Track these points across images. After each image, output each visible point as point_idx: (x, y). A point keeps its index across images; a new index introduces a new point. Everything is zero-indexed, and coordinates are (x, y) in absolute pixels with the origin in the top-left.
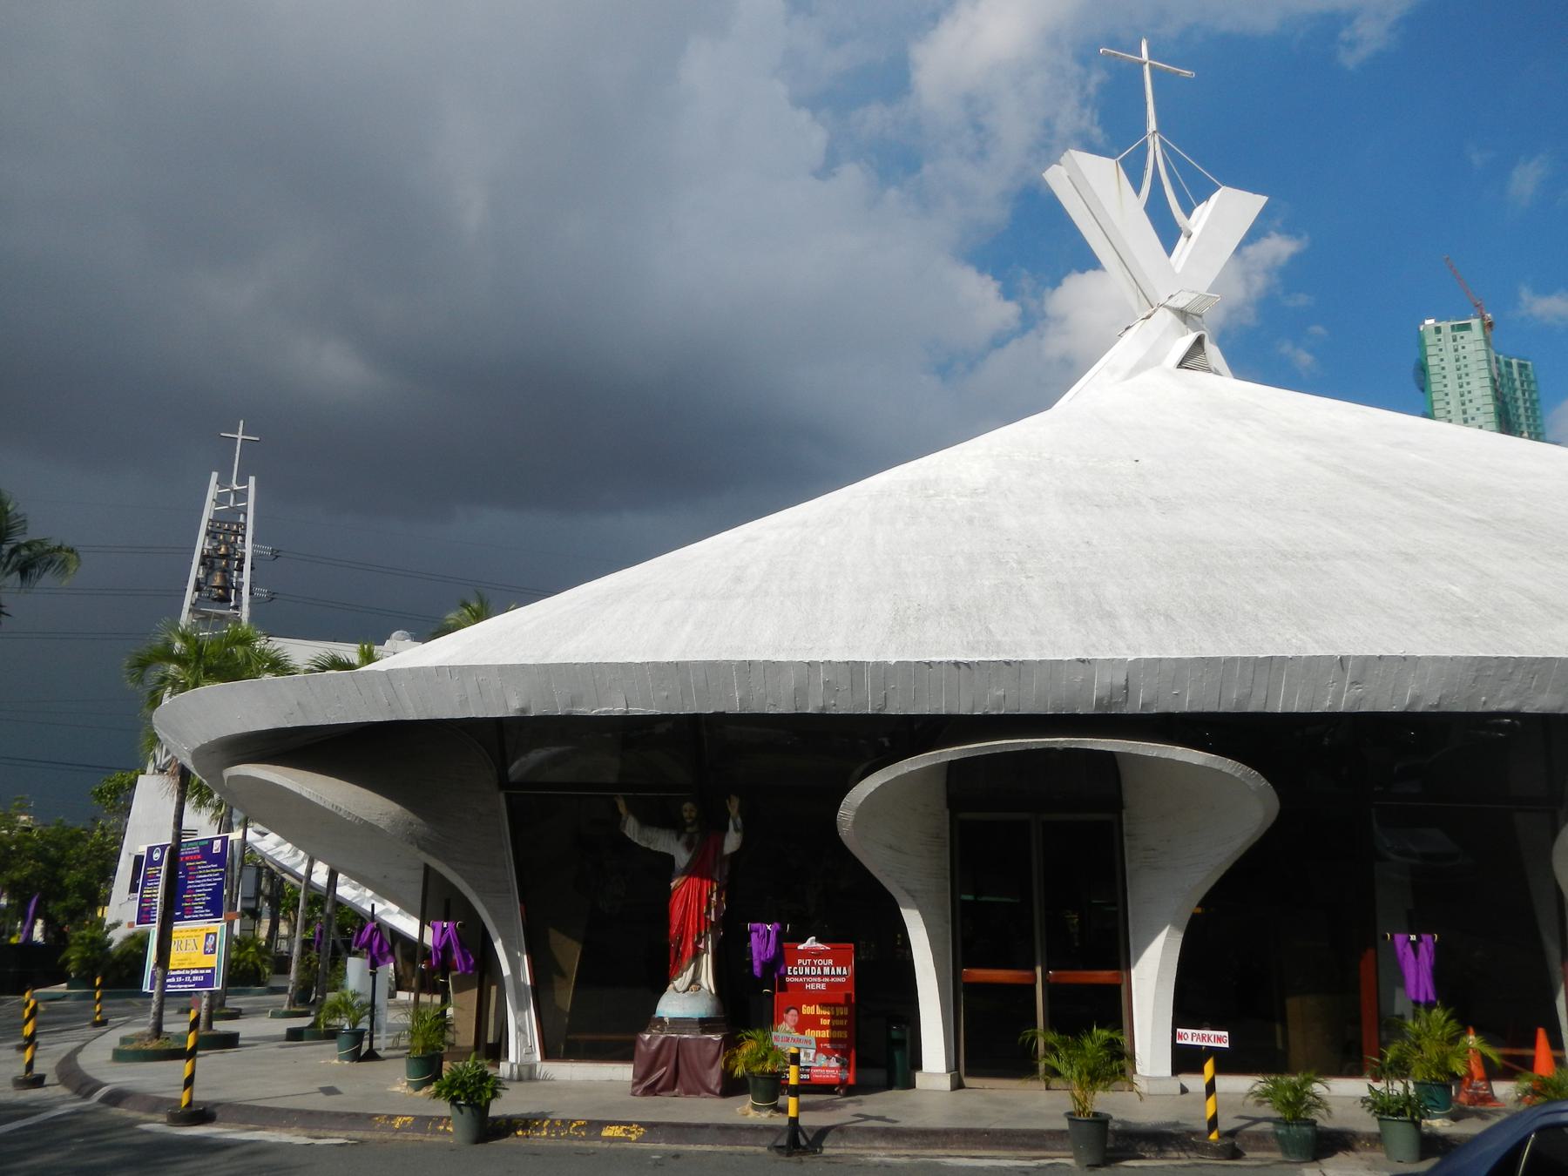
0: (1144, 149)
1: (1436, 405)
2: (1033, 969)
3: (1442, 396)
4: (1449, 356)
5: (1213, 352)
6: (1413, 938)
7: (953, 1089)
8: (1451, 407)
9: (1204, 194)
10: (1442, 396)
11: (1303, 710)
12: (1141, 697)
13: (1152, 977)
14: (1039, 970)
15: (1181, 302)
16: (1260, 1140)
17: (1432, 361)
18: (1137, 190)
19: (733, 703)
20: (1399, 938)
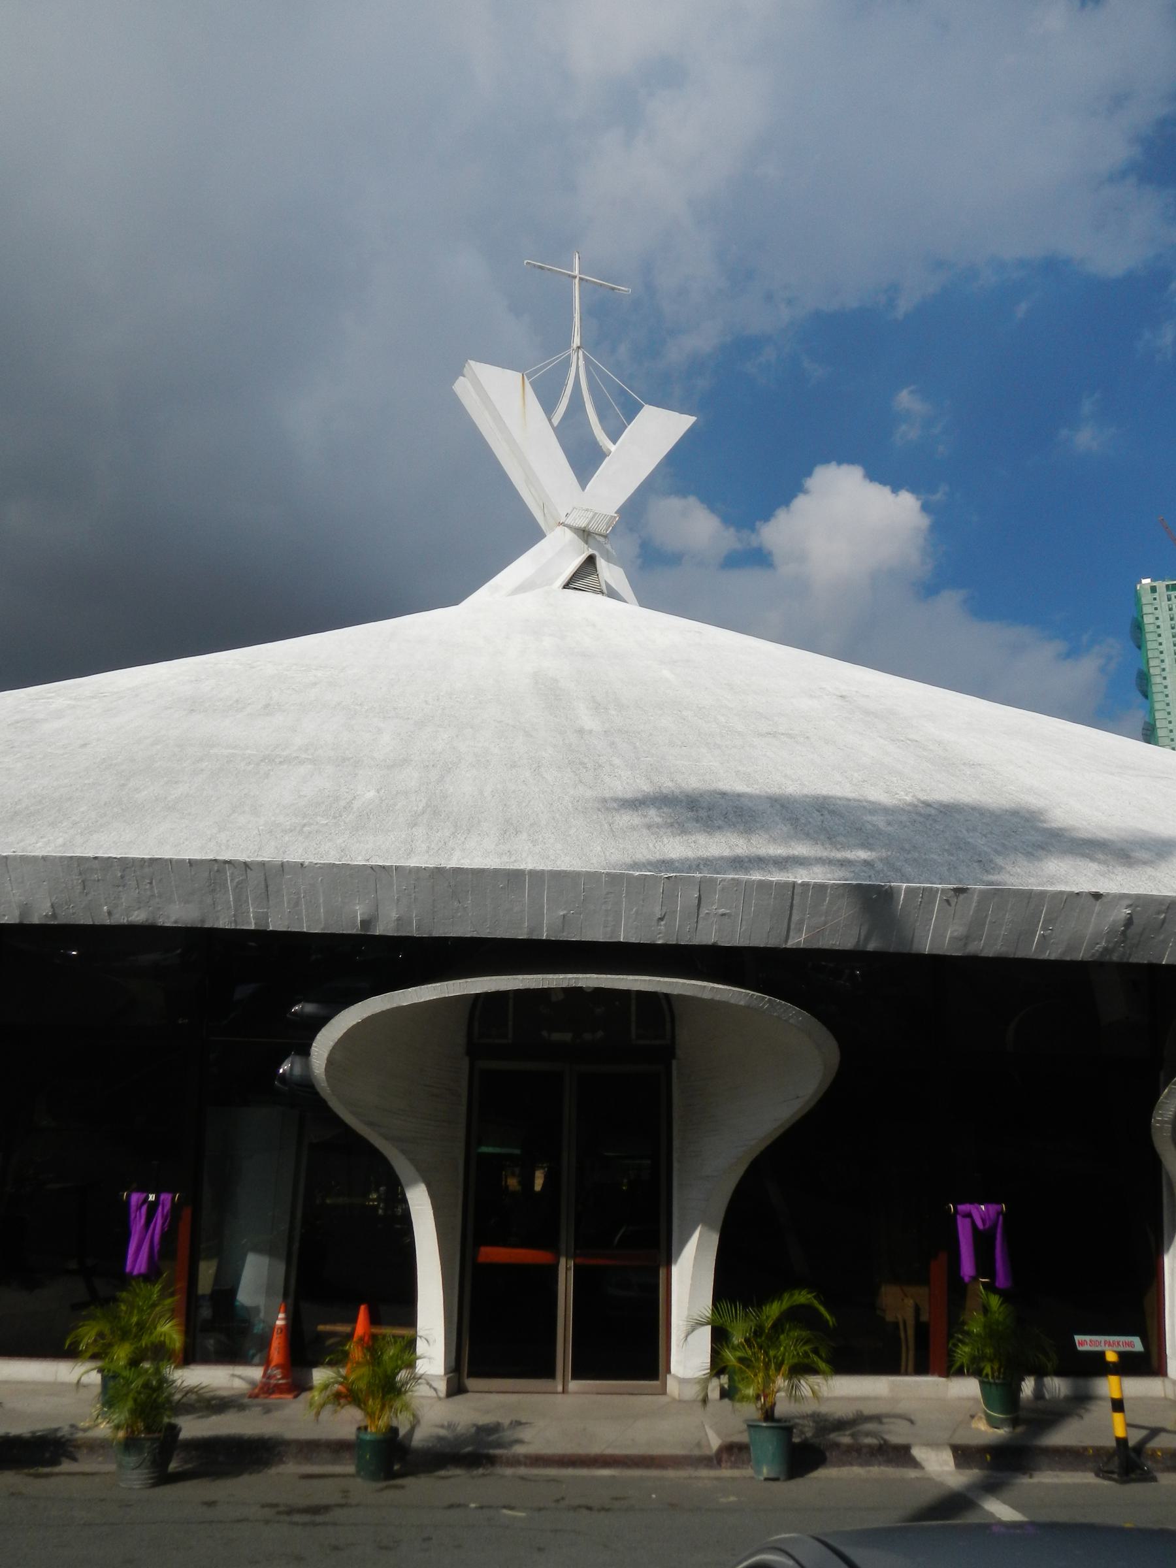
0: (567, 363)
1: (1152, 663)
3: (1157, 654)
4: (1164, 614)
5: (608, 572)
6: (152, 1197)
8: (1166, 665)
9: (631, 411)
10: (1157, 654)
12: (173, 919)
13: (690, 1280)
15: (581, 523)
16: (97, 1446)
17: (1148, 619)
18: (549, 408)
19: (176, 913)
20: (135, 1198)
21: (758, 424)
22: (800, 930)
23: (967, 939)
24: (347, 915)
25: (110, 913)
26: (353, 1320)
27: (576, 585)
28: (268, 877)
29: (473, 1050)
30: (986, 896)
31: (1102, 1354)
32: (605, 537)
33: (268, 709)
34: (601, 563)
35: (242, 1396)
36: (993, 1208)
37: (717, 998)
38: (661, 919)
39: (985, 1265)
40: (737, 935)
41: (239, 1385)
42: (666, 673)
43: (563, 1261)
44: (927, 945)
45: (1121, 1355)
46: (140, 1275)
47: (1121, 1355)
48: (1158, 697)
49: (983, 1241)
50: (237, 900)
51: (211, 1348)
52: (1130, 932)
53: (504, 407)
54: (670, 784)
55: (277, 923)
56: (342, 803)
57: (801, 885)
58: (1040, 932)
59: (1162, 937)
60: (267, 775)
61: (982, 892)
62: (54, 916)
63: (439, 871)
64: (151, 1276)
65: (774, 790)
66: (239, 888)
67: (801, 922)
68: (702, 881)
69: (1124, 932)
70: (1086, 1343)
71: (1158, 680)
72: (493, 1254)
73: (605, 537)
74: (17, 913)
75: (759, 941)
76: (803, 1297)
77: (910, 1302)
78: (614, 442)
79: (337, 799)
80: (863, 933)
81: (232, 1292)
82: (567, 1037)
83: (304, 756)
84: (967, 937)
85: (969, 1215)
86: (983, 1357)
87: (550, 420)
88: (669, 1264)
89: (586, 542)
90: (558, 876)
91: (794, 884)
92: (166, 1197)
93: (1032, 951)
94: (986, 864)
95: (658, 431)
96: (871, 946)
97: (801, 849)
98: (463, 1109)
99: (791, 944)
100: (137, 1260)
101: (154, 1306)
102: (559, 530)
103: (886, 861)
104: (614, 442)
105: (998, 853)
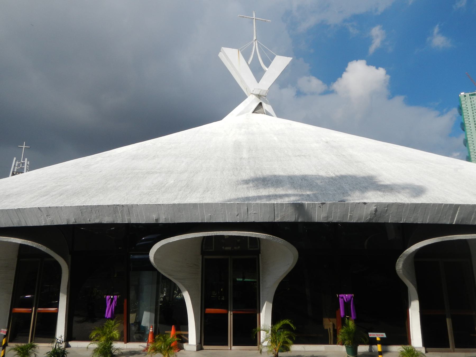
1: (465, 120)
2: (32, 308)
5: (266, 107)
6: (112, 297)
7: (197, 350)
10: (467, 117)
11: (431, 222)
13: (265, 317)
14: (34, 308)
15: (258, 93)
17: (463, 106)
18: (247, 59)
19: (107, 220)
20: (108, 297)
21: (322, 54)
22: (278, 217)
23: (327, 217)
24: (151, 218)
25: (90, 220)
26: (171, 330)
27: (256, 112)
28: (129, 208)
29: (203, 253)
30: (331, 205)
31: (376, 338)
32: (265, 96)
33: (154, 157)
34: (264, 104)
35: (141, 351)
36: (350, 295)
37: (257, 237)
38: (238, 215)
39: (347, 312)
40: (260, 219)
41: (142, 348)
42: (275, 138)
43: (229, 312)
44: (316, 220)
45: (381, 338)
46: (109, 318)
47: (381, 338)
48: (468, 131)
49: (347, 305)
50: (122, 215)
51: (135, 338)
52: (377, 213)
53: (233, 60)
54: (260, 174)
55: (133, 221)
56: (163, 185)
57: (279, 203)
58: (349, 215)
59: (387, 215)
60: (146, 178)
61: (330, 203)
62: (76, 222)
63: (174, 205)
64: (112, 318)
65: (291, 174)
66: (122, 212)
67: (278, 214)
68: (247, 204)
69: (375, 214)
70: (371, 335)
71: (468, 125)
72: (209, 310)
73: (265, 96)
74: (66, 222)
75: (266, 220)
76: (287, 322)
77: (331, 323)
78: (268, 67)
79: (162, 184)
80: (297, 216)
81: (140, 323)
82: (229, 248)
83: (158, 171)
84: (328, 217)
85: (342, 298)
86: (345, 340)
87: (247, 63)
88: (260, 313)
89: (259, 99)
90: (207, 204)
91: (274, 204)
92: (115, 297)
93: (348, 220)
94: (345, 193)
95: (280, 63)
96: (300, 221)
97: (290, 192)
98: (200, 270)
99: (275, 221)
100: (108, 314)
101: (113, 326)
102: (251, 95)
103: (315, 195)
104: (268, 67)
105: (350, 190)
